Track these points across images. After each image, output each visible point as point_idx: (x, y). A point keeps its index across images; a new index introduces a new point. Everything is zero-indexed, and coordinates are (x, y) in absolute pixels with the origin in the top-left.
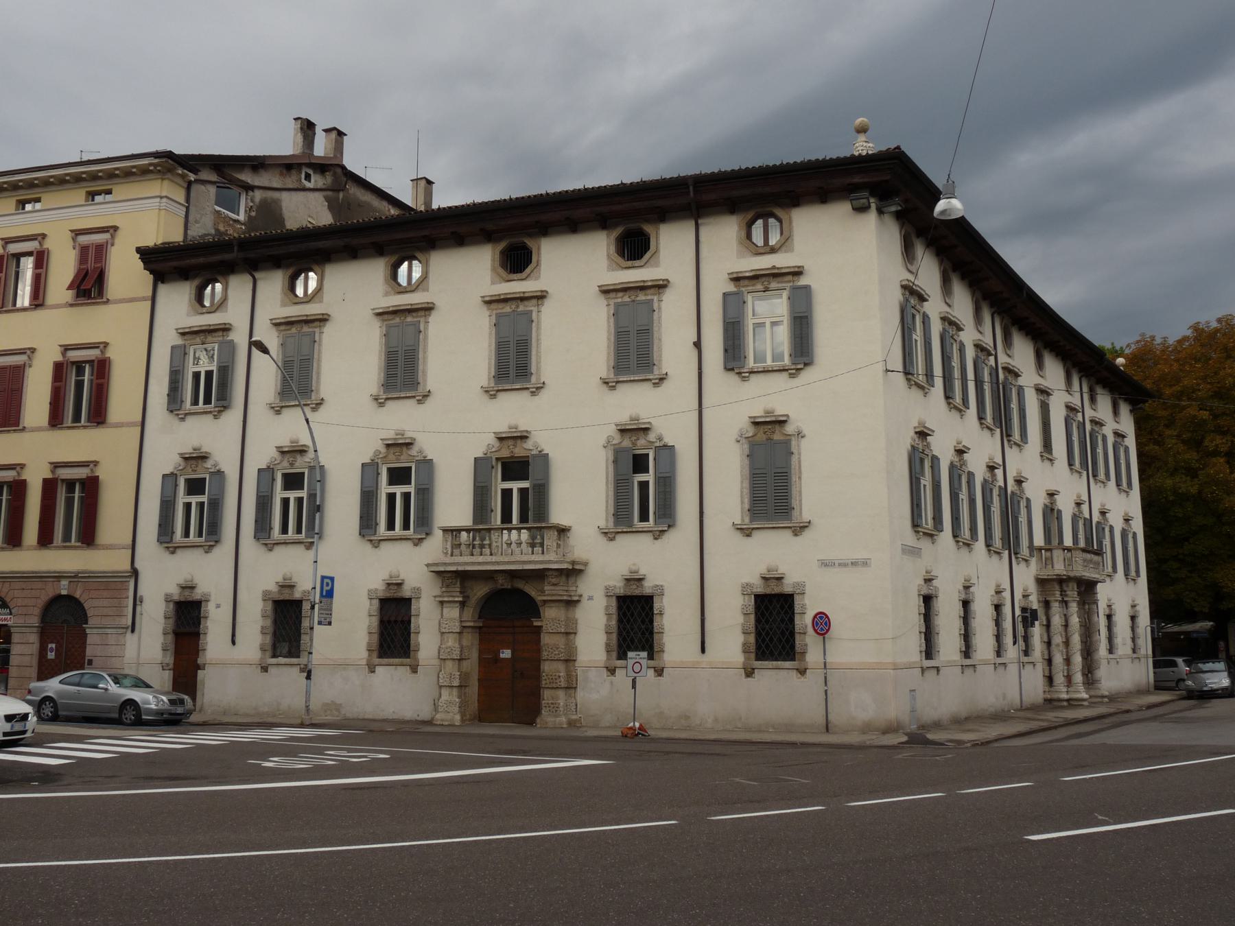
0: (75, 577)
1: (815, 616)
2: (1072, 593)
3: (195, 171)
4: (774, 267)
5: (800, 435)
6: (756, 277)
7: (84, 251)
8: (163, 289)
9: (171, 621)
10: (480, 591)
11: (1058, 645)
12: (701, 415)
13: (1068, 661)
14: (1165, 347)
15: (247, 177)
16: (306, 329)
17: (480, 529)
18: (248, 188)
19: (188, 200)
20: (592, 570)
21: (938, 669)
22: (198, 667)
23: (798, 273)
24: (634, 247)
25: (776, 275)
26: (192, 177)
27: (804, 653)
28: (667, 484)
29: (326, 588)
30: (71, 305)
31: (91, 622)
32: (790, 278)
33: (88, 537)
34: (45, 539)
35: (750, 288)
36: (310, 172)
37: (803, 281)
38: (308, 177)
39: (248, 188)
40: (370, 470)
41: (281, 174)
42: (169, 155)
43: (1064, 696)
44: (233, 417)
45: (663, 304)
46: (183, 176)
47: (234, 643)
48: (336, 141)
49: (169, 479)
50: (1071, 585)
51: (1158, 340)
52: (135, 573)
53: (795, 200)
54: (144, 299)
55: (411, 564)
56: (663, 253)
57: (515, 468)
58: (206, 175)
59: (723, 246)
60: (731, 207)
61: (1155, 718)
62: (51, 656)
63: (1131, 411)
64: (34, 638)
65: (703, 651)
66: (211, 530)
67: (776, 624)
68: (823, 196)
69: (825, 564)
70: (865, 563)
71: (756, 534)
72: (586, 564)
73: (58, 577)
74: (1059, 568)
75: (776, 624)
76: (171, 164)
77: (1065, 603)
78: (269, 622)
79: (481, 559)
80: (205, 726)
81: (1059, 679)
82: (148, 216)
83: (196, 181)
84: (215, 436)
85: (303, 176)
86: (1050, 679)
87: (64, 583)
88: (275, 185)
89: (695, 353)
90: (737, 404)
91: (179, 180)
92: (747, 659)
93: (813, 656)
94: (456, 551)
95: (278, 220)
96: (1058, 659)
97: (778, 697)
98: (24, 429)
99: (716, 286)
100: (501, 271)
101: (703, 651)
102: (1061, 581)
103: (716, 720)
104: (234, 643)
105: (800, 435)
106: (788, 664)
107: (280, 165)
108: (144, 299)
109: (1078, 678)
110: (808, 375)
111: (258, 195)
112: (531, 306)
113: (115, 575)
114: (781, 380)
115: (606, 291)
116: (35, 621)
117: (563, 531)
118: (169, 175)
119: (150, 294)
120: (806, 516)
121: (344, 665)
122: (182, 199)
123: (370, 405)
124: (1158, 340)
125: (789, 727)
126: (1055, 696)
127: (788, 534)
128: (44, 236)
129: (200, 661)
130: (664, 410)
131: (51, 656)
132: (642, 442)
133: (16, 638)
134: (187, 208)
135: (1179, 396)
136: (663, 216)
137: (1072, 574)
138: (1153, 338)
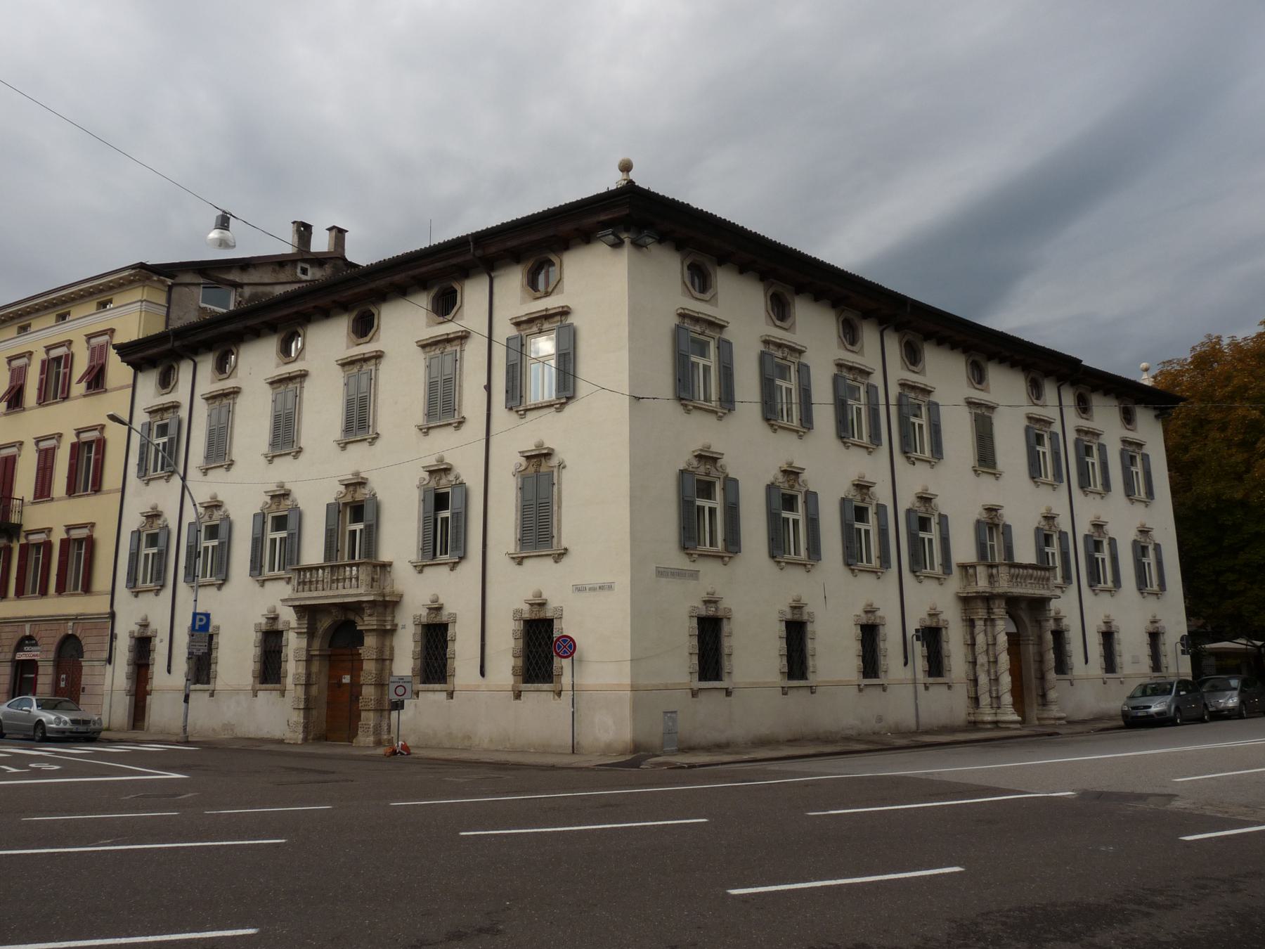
0: (76, 618)
1: (572, 639)
2: (999, 610)
3: (172, 277)
4: (547, 310)
5: (562, 466)
6: (531, 321)
7: (93, 351)
8: (140, 376)
9: (419, 662)
10: (325, 623)
11: (982, 665)
12: (484, 454)
13: (996, 680)
14: (1235, 346)
15: (235, 276)
16: (225, 401)
17: (333, 564)
18: (237, 285)
19: (169, 300)
20: (407, 600)
21: (728, 693)
22: (149, 693)
23: (565, 312)
24: (445, 305)
25: (547, 316)
26: (169, 282)
27: (560, 675)
28: (462, 518)
29: (198, 623)
30: (85, 396)
31: (86, 656)
32: (558, 318)
33: (87, 589)
34: (61, 589)
35: (528, 331)
36: (307, 266)
37: (570, 320)
38: (304, 271)
39: (237, 285)
40: (260, 518)
41: (274, 271)
42: (142, 266)
43: (989, 718)
44: (176, 481)
45: (466, 354)
46: (163, 282)
47: (169, 671)
48: (336, 237)
49: (137, 534)
50: (997, 602)
51: (1226, 341)
52: (112, 615)
53: (565, 244)
54: (127, 386)
55: (276, 598)
56: (466, 307)
57: (357, 510)
58: (187, 278)
59: (511, 293)
60: (514, 257)
61: (848, 739)
62: (63, 684)
63: (1157, 417)
64: (50, 670)
65: (483, 674)
66: (159, 575)
67: (542, 647)
68: (586, 237)
69: (579, 589)
70: (610, 587)
71: (527, 563)
72: (401, 596)
73: (66, 619)
74: (982, 584)
75: (542, 647)
76: (145, 273)
77: (990, 621)
78: (520, 662)
79: (315, 594)
80: (110, 742)
81: (985, 700)
82: (131, 319)
83: (174, 285)
84: (165, 495)
85: (299, 270)
86: (976, 700)
87: (70, 624)
88: (266, 281)
89: (485, 393)
90: (513, 440)
91: (161, 286)
92: (515, 682)
93: (566, 680)
94: (301, 588)
95: (235, 308)
96: (983, 679)
97: (538, 721)
98: (52, 499)
99: (504, 331)
100: (353, 336)
101: (483, 674)
102: (988, 599)
103: (491, 740)
104: (169, 671)
105: (562, 466)
106: (546, 686)
107: (272, 263)
108: (127, 386)
109: (1007, 699)
110: (571, 408)
111: (247, 291)
112: (370, 366)
113: (98, 617)
114: (549, 416)
115: (424, 346)
116: (51, 656)
117: (386, 566)
118: (147, 282)
119: (131, 382)
120: (565, 544)
121: (237, 691)
122: (163, 301)
123: (263, 461)
124: (1226, 341)
125: (545, 750)
126: (980, 718)
127: (550, 561)
128: (70, 342)
129: (148, 688)
130: (460, 450)
131: (63, 684)
132: (443, 482)
133: (41, 671)
134: (168, 308)
135: (1232, 397)
136: (466, 272)
137: (996, 591)
138: (1219, 338)
